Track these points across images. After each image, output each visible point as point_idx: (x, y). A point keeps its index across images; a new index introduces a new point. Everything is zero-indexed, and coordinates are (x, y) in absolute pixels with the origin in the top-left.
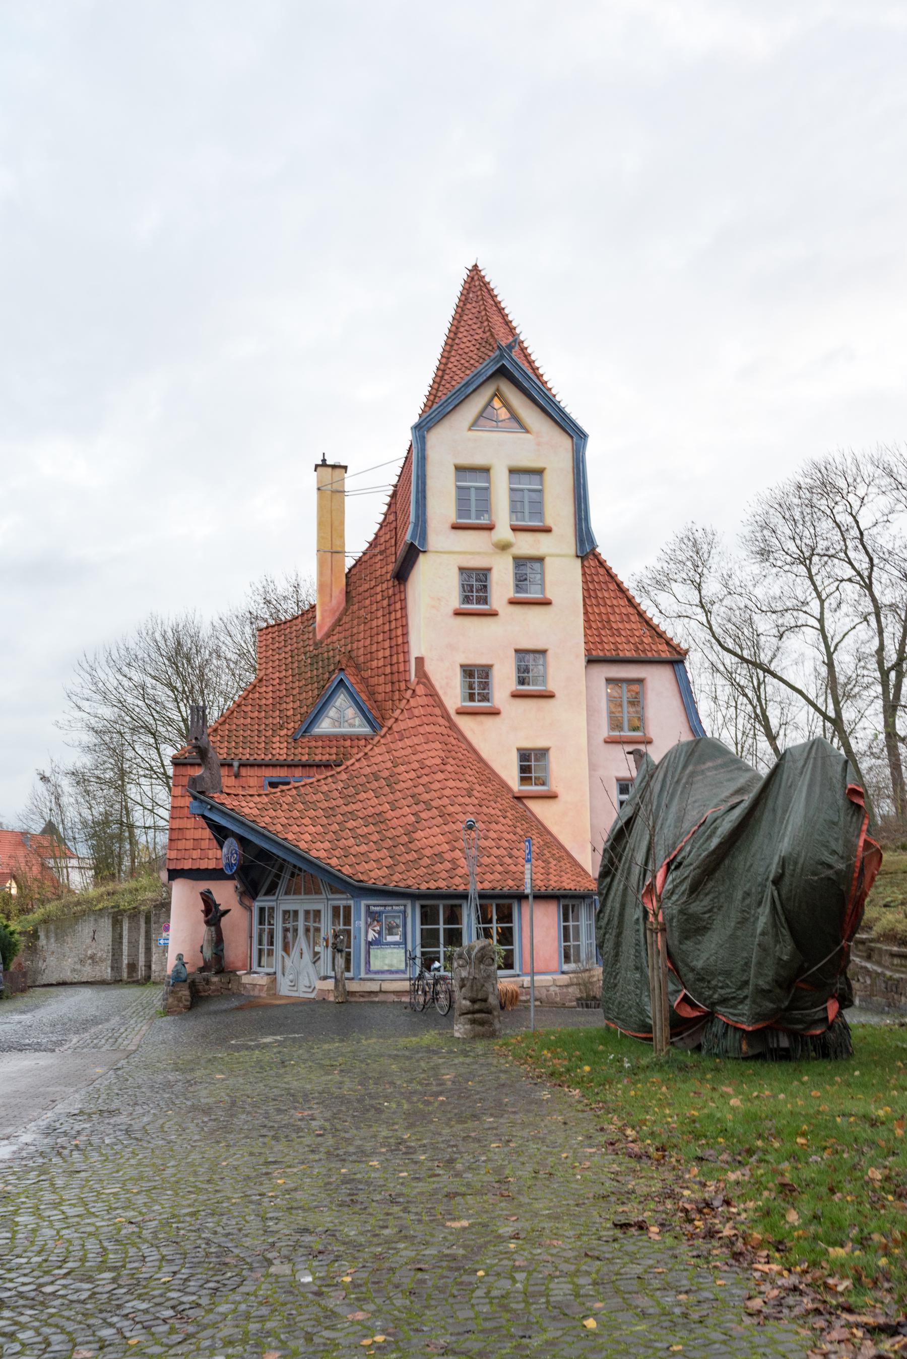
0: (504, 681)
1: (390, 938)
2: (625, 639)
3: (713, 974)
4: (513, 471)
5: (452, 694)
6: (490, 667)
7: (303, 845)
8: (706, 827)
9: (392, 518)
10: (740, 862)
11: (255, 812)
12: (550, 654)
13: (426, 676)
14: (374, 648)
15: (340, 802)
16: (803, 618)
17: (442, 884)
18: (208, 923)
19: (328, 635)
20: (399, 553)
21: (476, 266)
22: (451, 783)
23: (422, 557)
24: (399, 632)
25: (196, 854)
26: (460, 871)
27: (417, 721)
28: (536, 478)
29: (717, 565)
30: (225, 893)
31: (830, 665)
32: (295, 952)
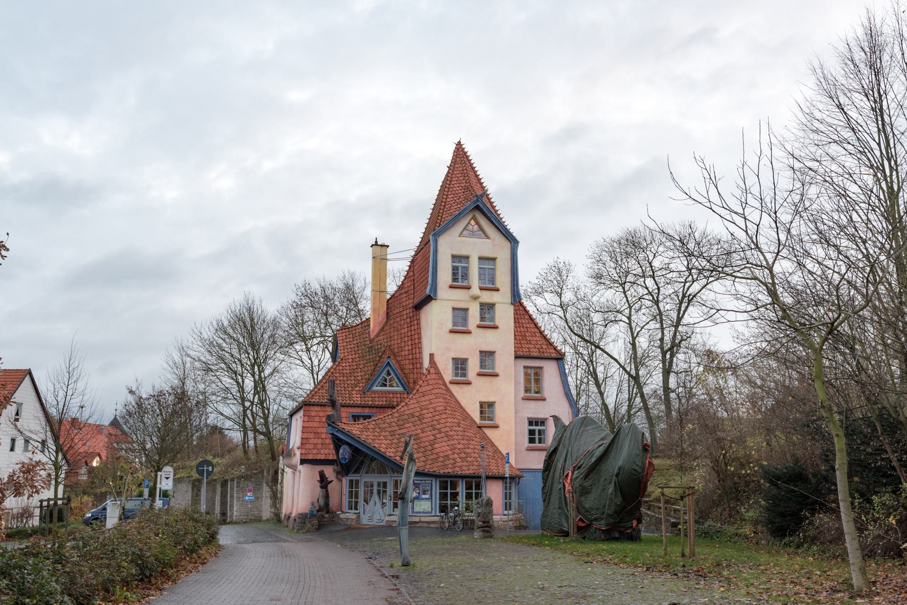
0: (473, 366)
1: (424, 496)
2: (533, 346)
3: (592, 509)
4: (480, 258)
5: (448, 374)
6: (466, 360)
7: (382, 450)
8: (590, 453)
9: (411, 274)
10: (603, 467)
11: (358, 433)
12: (497, 355)
13: (435, 363)
14: (403, 344)
15: (397, 428)
16: (620, 316)
17: (451, 471)
18: (321, 487)
19: (377, 336)
20: (416, 294)
21: (459, 142)
22: (449, 420)
23: (433, 302)
24: (416, 337)
25: (315, 451)
26: (458, 464)
27: (431, 387)
28: (492, 262)
29: (571, 282)
30: (329, 472)
31: (634, 345)
32: (371, 503)
